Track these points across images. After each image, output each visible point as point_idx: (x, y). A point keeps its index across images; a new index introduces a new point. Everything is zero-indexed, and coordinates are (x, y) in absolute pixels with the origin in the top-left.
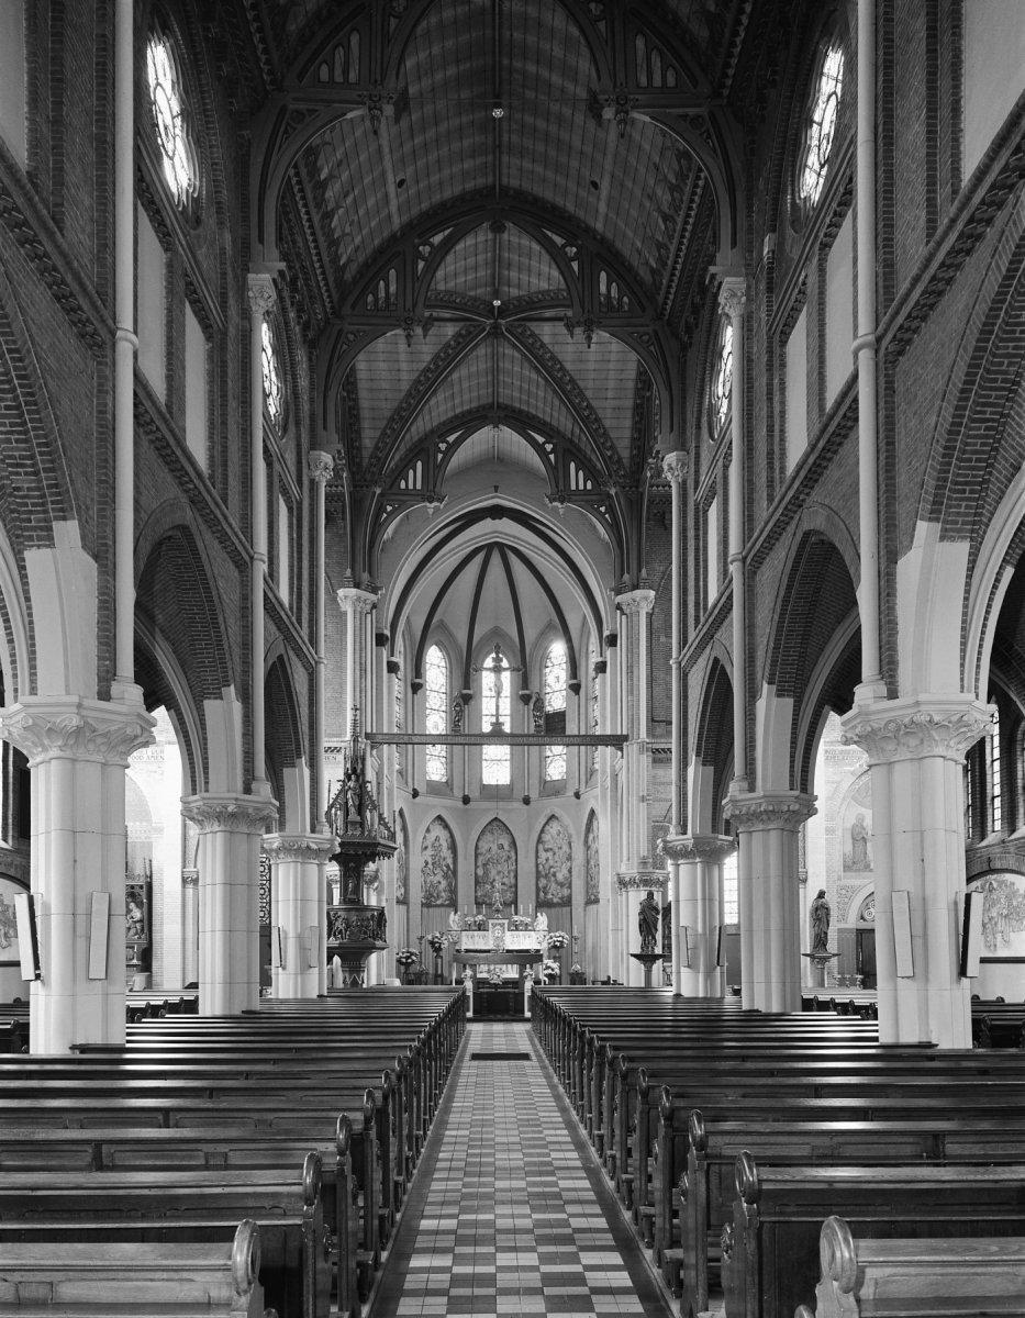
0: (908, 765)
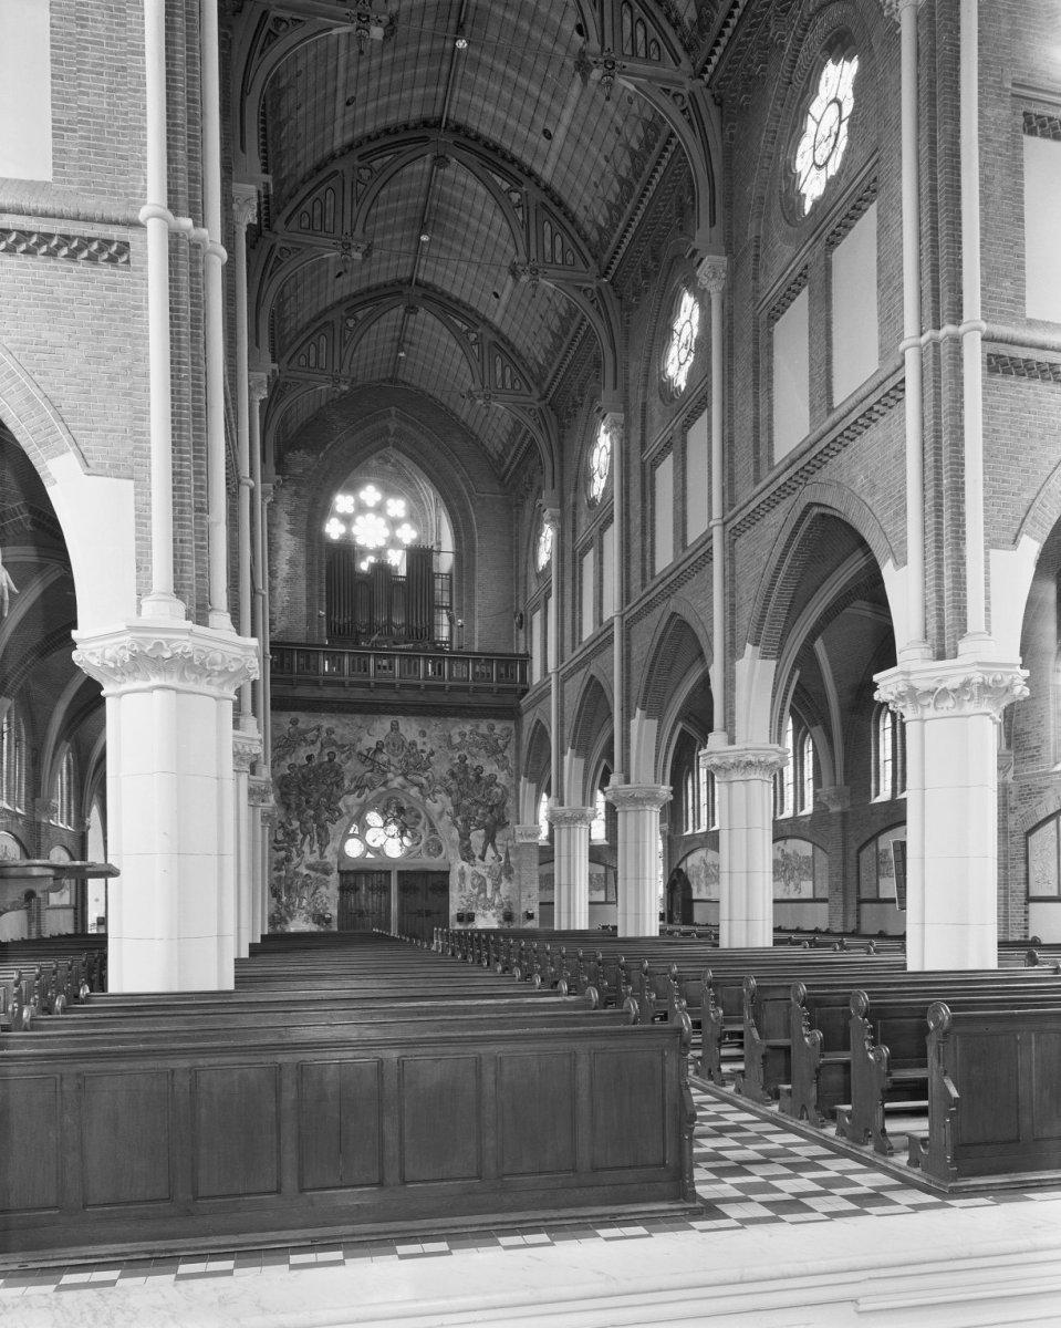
0: (633, 813)
